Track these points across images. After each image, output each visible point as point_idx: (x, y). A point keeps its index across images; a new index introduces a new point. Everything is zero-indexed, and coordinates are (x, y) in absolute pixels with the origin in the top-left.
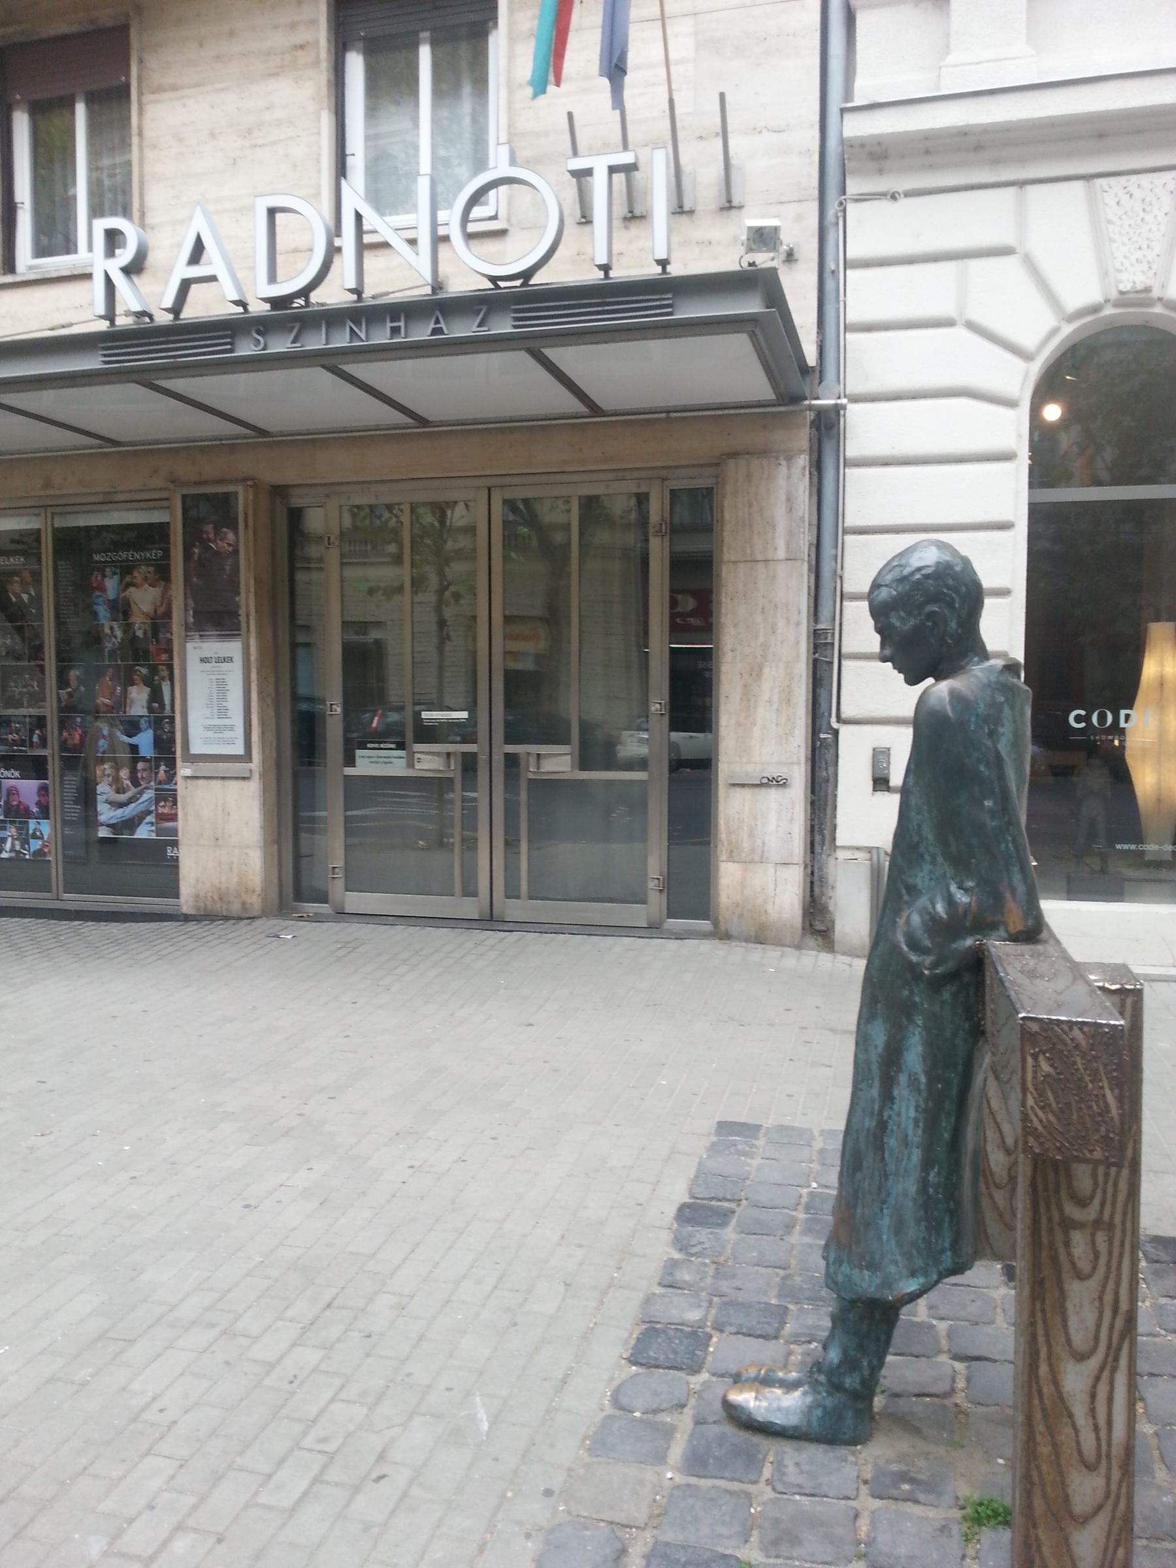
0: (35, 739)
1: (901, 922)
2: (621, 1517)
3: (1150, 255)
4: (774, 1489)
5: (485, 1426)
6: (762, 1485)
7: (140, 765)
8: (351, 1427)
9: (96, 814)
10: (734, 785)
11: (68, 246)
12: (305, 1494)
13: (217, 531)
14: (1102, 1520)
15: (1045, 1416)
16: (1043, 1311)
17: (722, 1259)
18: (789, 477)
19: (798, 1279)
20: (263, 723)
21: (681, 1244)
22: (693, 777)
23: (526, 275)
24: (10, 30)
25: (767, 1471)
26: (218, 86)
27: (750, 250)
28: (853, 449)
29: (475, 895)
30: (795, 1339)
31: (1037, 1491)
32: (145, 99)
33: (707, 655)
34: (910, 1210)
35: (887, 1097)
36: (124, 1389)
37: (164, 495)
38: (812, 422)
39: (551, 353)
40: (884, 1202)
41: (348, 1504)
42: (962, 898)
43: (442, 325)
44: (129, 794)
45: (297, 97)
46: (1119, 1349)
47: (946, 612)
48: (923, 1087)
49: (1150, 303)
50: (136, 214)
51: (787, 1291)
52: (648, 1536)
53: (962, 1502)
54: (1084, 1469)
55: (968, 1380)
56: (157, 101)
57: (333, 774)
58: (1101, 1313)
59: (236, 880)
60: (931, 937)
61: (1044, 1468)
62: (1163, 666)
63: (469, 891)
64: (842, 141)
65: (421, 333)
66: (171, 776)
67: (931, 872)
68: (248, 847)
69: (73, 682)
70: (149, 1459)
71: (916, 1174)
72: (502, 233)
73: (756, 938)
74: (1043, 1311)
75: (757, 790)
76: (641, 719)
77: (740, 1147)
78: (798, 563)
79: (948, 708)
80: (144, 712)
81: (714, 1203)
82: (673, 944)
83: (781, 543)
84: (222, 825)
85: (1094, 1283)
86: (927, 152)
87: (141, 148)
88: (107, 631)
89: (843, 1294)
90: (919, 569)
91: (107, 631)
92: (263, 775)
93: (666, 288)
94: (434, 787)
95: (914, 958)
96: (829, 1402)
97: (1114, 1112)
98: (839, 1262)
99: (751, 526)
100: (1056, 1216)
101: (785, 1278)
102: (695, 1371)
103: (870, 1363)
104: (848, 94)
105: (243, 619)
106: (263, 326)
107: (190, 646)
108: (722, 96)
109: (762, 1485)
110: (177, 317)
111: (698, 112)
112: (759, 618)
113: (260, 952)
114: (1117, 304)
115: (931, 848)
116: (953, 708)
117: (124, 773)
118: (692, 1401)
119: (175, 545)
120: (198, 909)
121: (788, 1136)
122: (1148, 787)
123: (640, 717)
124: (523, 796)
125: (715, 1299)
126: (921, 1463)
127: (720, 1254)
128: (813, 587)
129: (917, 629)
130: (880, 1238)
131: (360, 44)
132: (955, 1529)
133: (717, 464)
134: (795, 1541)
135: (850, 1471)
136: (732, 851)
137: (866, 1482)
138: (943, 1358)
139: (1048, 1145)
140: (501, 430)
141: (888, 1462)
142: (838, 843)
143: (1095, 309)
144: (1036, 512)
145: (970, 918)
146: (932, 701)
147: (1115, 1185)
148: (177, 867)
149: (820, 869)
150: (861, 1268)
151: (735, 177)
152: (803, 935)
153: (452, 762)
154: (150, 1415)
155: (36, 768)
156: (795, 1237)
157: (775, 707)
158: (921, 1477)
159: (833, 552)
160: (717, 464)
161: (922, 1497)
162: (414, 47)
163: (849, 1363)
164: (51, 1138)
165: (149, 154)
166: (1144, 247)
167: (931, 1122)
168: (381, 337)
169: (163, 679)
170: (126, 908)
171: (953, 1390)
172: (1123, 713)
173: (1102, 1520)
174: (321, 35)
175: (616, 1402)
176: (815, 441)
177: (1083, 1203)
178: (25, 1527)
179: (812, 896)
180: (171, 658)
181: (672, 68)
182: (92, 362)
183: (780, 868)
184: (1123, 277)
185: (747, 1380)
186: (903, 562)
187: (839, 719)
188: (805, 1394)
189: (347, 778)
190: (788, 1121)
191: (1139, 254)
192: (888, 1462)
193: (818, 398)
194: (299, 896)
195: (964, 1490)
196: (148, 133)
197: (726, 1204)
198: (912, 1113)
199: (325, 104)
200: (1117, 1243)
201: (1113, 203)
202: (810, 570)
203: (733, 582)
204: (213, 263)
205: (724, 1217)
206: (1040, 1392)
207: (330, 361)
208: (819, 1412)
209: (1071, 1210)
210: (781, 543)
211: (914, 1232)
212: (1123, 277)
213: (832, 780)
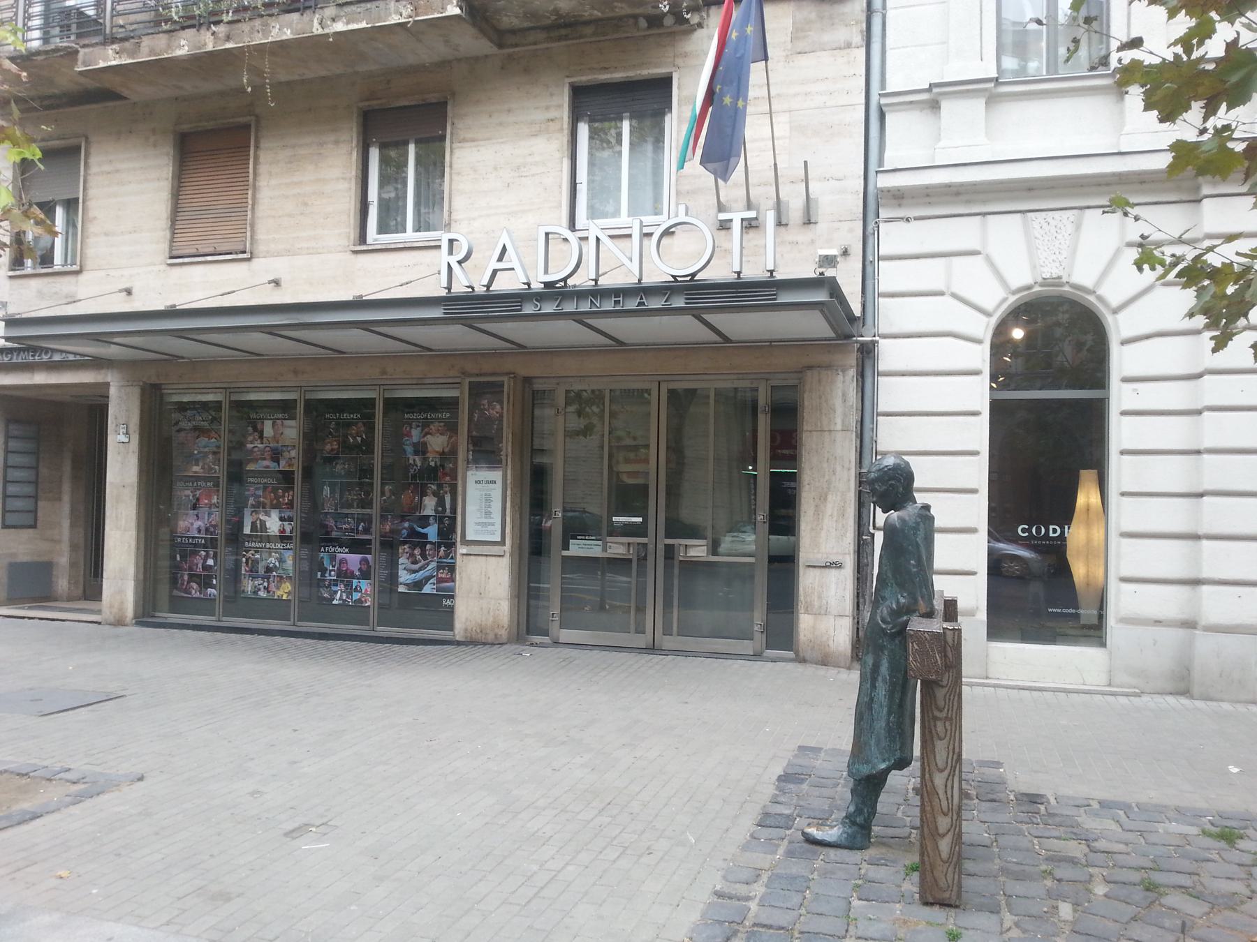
3: (1061, 258)
7: (428, 547)
13: (490, 404)
14: (950, 835)
20: (513, 521)
21: (778, 788)
22: (783, 566)
23: (693, 275)
24: (375, 102)
27: (820, 266)
28: (883, 366)
33: (793, 477)
35: (874, 687)
42: (902, 600)
45: (546, 151)
49: (1062, 285)
57: (557, 553)
63: (640, 630)
65: (632, 304)
69: (388, 494)
80: (432, 513)
82: (770, 665)
83: (839, 421)
84: (484, 584)
85: (945, 741)
93: (772, 285)
94: (618, 564)
98: (854, 763)
104: (881, 162)
105: (503, 458)
106: (539, 297)
107: (469, 473)
108: (806, 162)
112: (825, 465)
121: (836, 752)
124: (676, 571)
129: (887, 490)
140: (669, 349)
143: (1029, 288)
146: (890, 521)
151: (812, 205)
155: (358, 546)
156: (839, 788)
163: (859, 811)
165: (455, 177)
168: (608, 306)
172: (1051, 527)
173: (950, 835)
174: (565, 114)
175: (752, 836)
182: (437, 313)
184: (1045, 270)
187: (874, 527)
191: (1054, 257)
194: (528, 633)
195: (908, 863)
196: (455, 166)
203: (809, 442)
204: (512, 259)
205: (802, 781)
207: (578, 317)
210: (839, 421)
211: (884, 743)
212: (1045, 270)
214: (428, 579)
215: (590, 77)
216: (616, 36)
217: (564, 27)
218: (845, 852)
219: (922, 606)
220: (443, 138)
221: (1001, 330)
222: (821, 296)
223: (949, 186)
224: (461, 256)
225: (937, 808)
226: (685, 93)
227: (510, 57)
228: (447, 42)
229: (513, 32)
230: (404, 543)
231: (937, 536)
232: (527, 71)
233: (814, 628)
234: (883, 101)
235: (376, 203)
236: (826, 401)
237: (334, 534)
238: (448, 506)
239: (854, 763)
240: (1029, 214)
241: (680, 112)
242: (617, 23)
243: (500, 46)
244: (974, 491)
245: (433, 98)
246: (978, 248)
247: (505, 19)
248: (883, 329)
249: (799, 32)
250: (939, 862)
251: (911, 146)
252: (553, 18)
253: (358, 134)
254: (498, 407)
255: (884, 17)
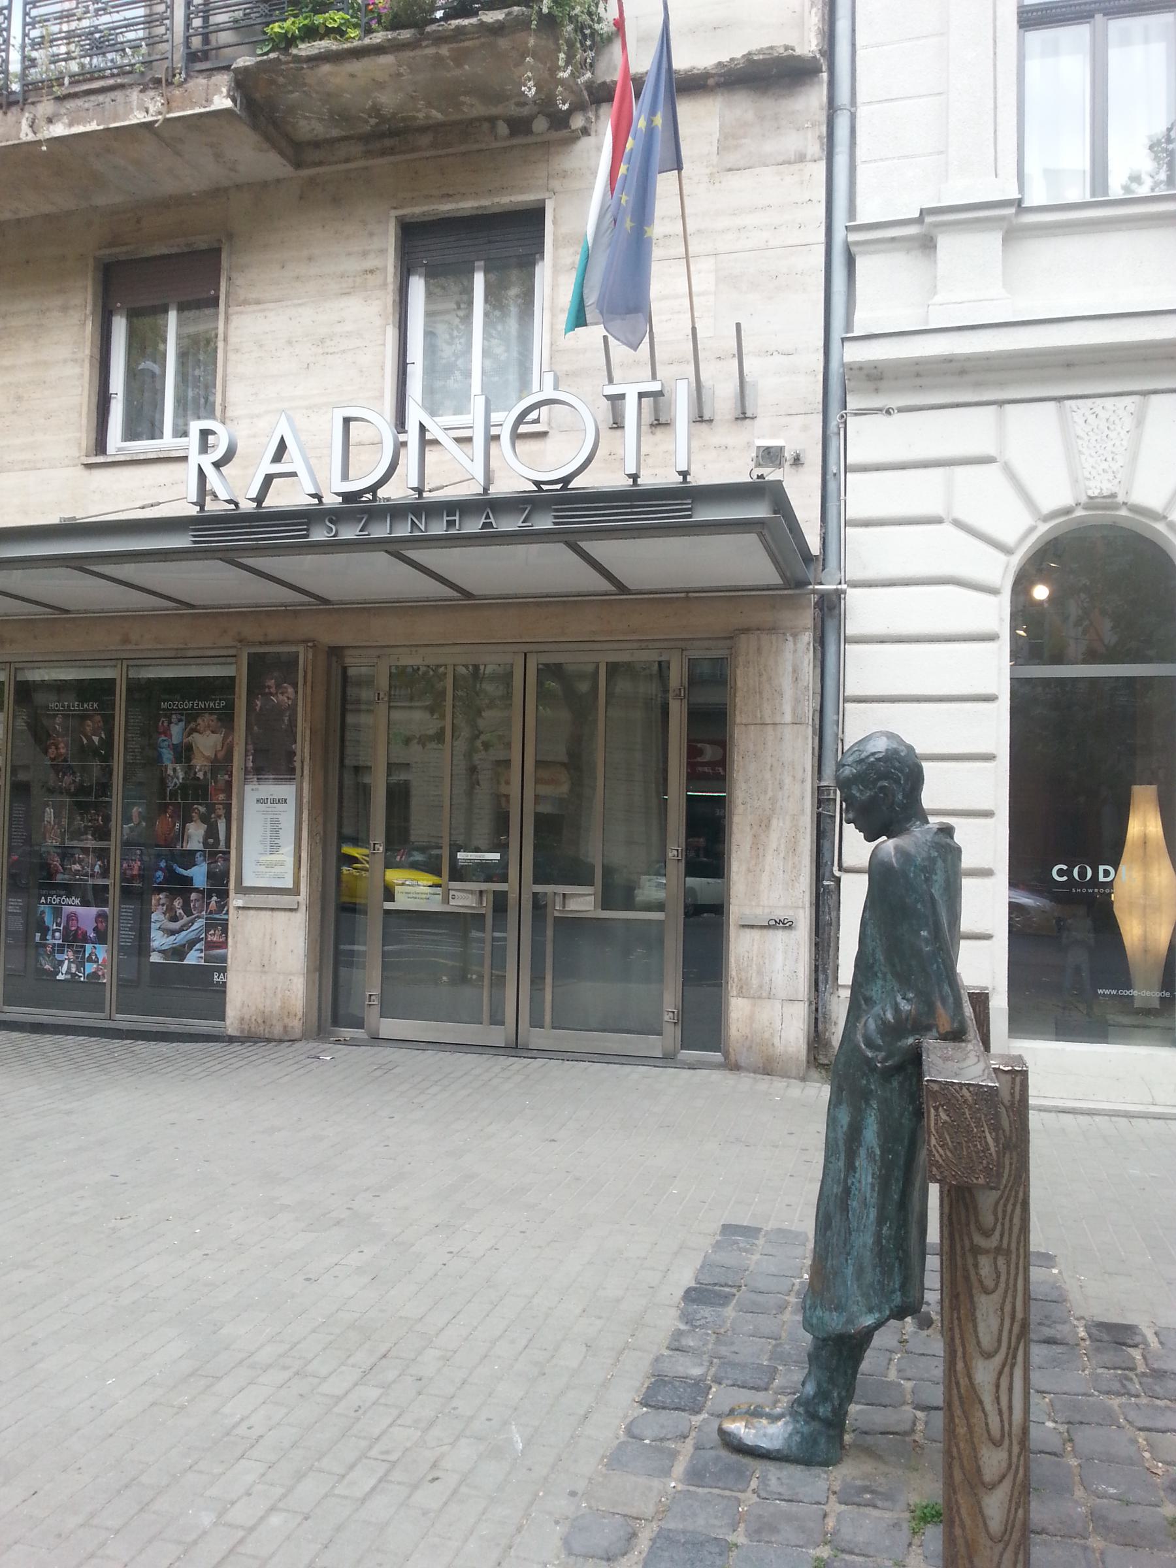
0: (97, 869)
1: (860, 1025)
2: (633, 1512)
3: (1115, 466)
4: (759, 1496)
5: (520, 1446)
6: (749, 1493)
7: (193, 896)
8: (408, 1445)
9: (149, 940)
10: (743, 926)
11: (155, 432)
12: (374, 1489)
13: (278, 686)
14: (1006, 1486)
15: (962, 1404)
16: (959, 1319)
17: (722, 1331)
18: (795, 651)
19: (787, 1347)
20: (311, 859)
21: (687, 1318)
22: (706, 921)
23: (566, 480)
24: (117, 250)
25: (754, 1484)
26: (296, 301)
27: (759, 465)
28: (852, 627)
29: (503, 1023)
30: (782, 1391)
31: (956, 1463)
32: (231, 310)
34: (868, 1257)
35: (851, 1167)
36: (216, 1412)
37: (232, 652)
38: (816, 604)
39: (585, 545)
40: (848, 1254)
41: (409, 1497)
43: (492, 520)
44: (181, 923)
46: (1016, 1349)
47: (894, 786)
48: (877, 1158)
49: (1116, 507)
50: (218, 413)
51: (775, 1355)
52: (655, 1526)
53: (912, 1508)
54: (991, 1445)
55: (926, 1423)
56: (241, 313)
58: (1002, 1320)
59: (279, 1004)
60: (882, 1038)
61: (962, 1445)
62: (1145, 826)
63: (497, 1019)
64: (843, 365)
65: (473, 526)
66: (223, 905)
67: (883, 987)
68: (291, 974)
69: (136, 819)
70: (242, 1461)
71: (872, 1228)
72: (544, 434)
73: (764, 1069)
74: (959, 1319)
75: (765, 931)
76: (659, 867)
77: (741, 1245)
78: (803, 727)
79: (894, 860)
80: (200, 847)
81: (716, 1288)
82: (686, 1073)
83: (787, 709)
84: (269, 954)
85: (996, 1297)
86: (918, 375)
87: (226, 352)
88: (170, 772)
89: (817, 1334)
90: (873, 754)
91: (170, 772)
92: (309, 907)
95: (870, 1054)
96: (806, 1430)
97: (993, 1150)
98: (813, 1307)
99: (761, 693)
100: (967, 1242)
101: (776, 1346)
102: (697, 1412)
103: (839, 1394)
104: (849, 326)
105: (298, 765)
106: (334, 516)
108: (738, 325)
109: (749, 1493)
110: (259, 505)
111: (716, 336)
112: (768, 775)
113: (302, 1071)
114: (1087, 507)
115: (883, 968)
116: (897, 860)
117: (178, 903)
118: (693, 1434)
119: (240, 697)
120: (242, 1031)
121: (784, 1236)
122: (1136, 939)
123: (658, 862)
124: (550, 933)
125: (715, 1360)
126: (882, 1480)
127: (720, 1327)
128: (817, 748)
129: (873, 800)
130: (845, 1283)
131: (423, 270)
132: (905, 1525)
133: (731, 638)
134: (774, 1530)
135: (822, 1484)
136: (742, 987)
137: (835, 1493)
138: (908, 1408)
139: (946, 1173)
140: (538, 604)
141: (854, 1479)
142: (840, 982)
143: (1068, 511)
144: (1017, 684)
145: (910, 1022)
146: (881, 854)
147: (1011, 1220)
148: (225, 992)
149: (824, 1006)
150: (831, 1311)
152: (808, 1067)
153: (484, 899)
154: (242, 1430)
155: (99, 896)
157: (782, 855)
158: (879, 1489)
159: (835, 718)
160: (731, 638)
161: (879, 1503)
162: (471, 272)
163: (823, 1395)
164: (130, 1221)
165: (232, 357)
166: (1109, 459)
167: (884, 1182)
168: (438, 528)
169: (219, 817)
170: (172, 1028)
171: (913, 1431)
172: (1101, 868)
173: (1006, 1486)
174: (390, 262)
175: (629, 1431)
176: (819, 620)
177: (987, 1234)
178: (147, 1504)
179: (816, 1031)
180: (229, 797)
181: (695, 299)
182: (183, 541)
183: (785, 1003)
184: (1092, 484)
185: (740, 1414)
186: (861, 748)
187: (841, 868)
188: (786, 1423)
189: (387, 912)
190: (786, 1225)
191: (1105, 465)
192: (854, 1479)
193: (821, 584)
194: (336, 1021)
195: (914, 1499)
196: (232, 340)
197: (727, 1289)
198: (870, 1180)
199: (390, 321)
200: (1013, 1266)
201: (1081, 421)
202: (814, 733)
203: (744, 740)
204: (294, 460)
205: (725, 1299)
206: (957, 1383)
207: (394, 548)
208: (797, 1438)
209: (978, 1240)
210: (787, 709)
211: (869, 1276)
212: (1092, 484)
213: (834, 923)
214: (192, 944)
215: (425, 208)
216: (463, 148)
217: (389, 136)
218: (797, 1471)
219: (944, 1021)
220: (214, 302)
221: (1022, 583)
222: (759, 511)
223: (949, 360)
224: (217, 454)
225: (979, 1430)
226: (564, 230)
227: (312, 182)
228: (218, 156)
229: (316, 144)
230: (159, 890)
231: (966, 883)
232: (336, 201)
233: (752, 1018)
234: (853, 237)
235: (120, 396)
236: (770, 679)
237: (60, 878)
238: (222, 836)
239: (813, 1307)
240: (1068, 403)
241: (555, 258)
242: (466, 129)
243: (298, 165)
244: (988, 814)
245: (202, 242)
246: (991, 451)
247: (303, 123)
248: (853, 573)
249: (728, 140)
250: (983, 1540)
251: (889, 298)
252: (373, 121)
253: (95, 295)
254: (290, 690)
255: (853, 117)
